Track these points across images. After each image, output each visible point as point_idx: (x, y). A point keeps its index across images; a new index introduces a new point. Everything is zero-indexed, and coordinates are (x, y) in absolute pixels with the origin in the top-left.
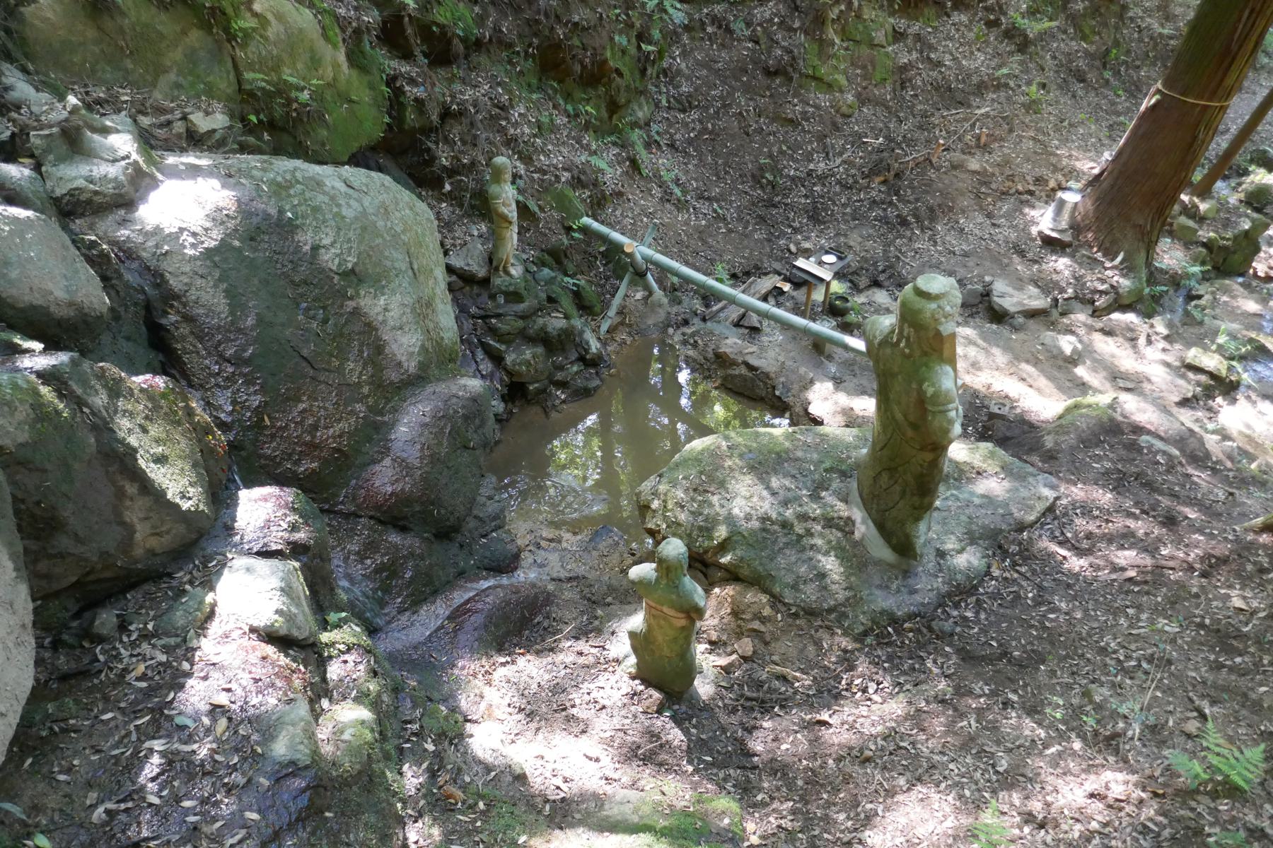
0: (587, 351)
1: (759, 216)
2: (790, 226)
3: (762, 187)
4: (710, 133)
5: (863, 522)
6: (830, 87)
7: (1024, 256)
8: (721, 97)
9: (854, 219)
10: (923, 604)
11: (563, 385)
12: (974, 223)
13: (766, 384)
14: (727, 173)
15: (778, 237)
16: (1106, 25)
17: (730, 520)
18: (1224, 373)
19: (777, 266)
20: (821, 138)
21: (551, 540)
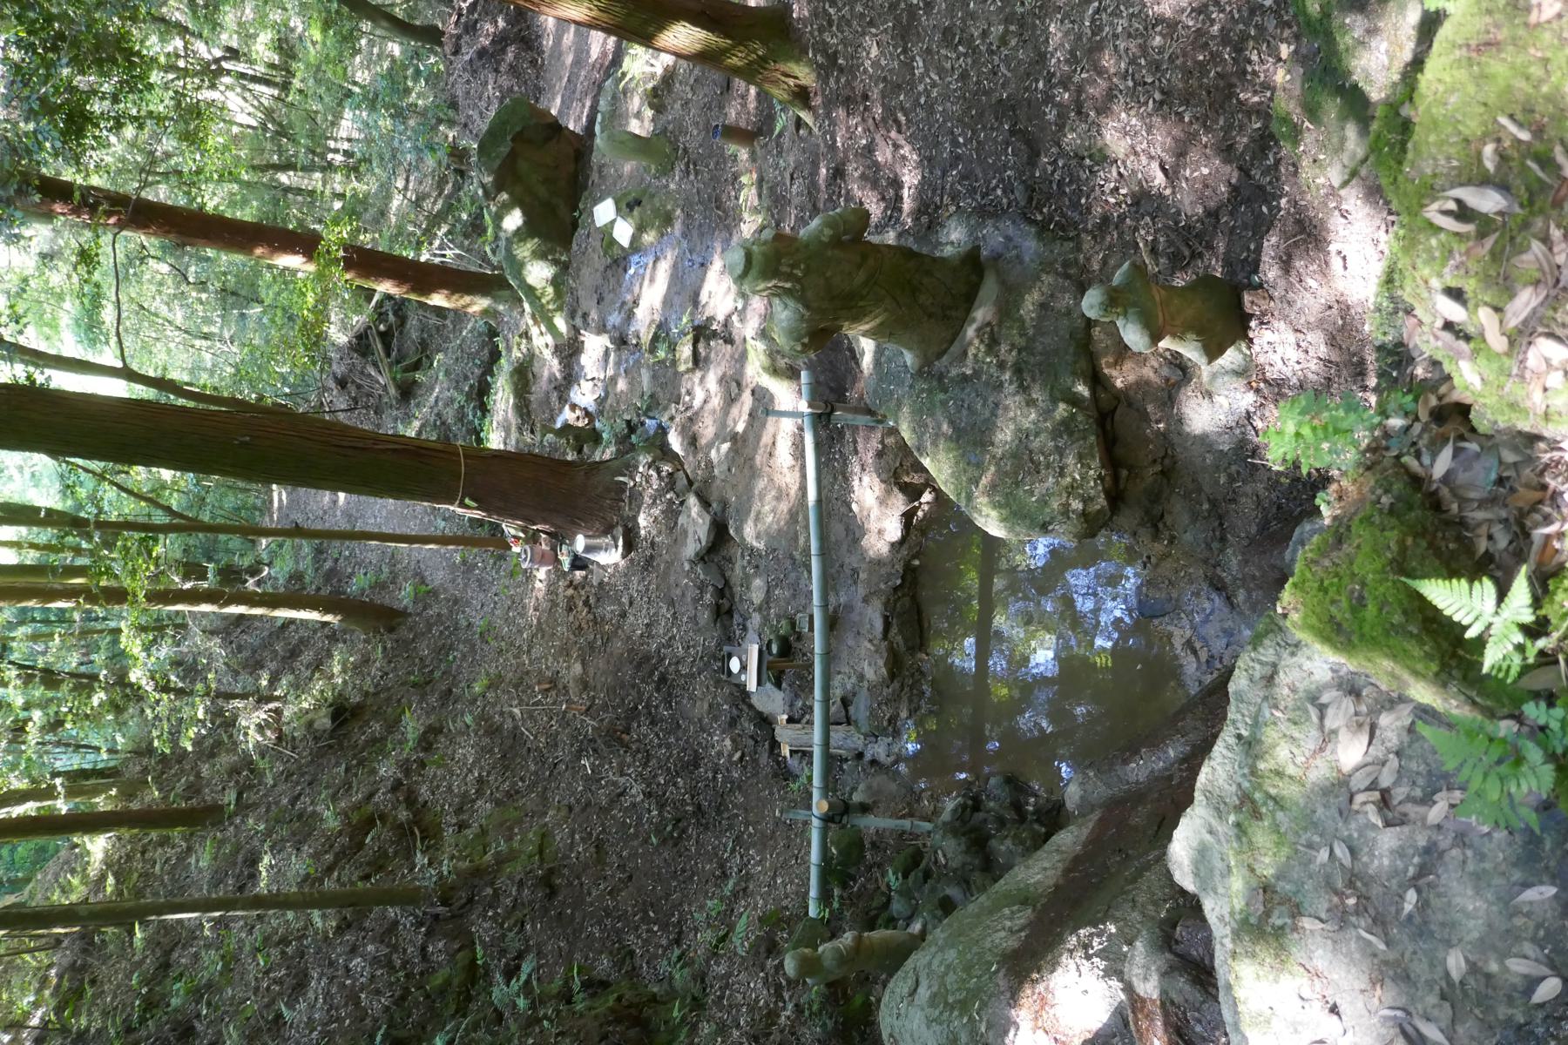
0: (964, 807)
1: (719, 812)
2: (714, 778)
3: (684, 831)
4: (646, 912)
5: (974, 320)
6: (545, 836)
7: (652, 557)
8: (599, 923)
9: (679, 726)
10: (1014, 222)
11: (1018, 807)
12: (636, 622)
13: (896, 602)
14: (684, 871)
15: (732, 782)
16: (389, 699)
17: (1047, 413)
18: (690, 337)
19: (764, 759)
20: (604, 811)
21: (1195, 652)
